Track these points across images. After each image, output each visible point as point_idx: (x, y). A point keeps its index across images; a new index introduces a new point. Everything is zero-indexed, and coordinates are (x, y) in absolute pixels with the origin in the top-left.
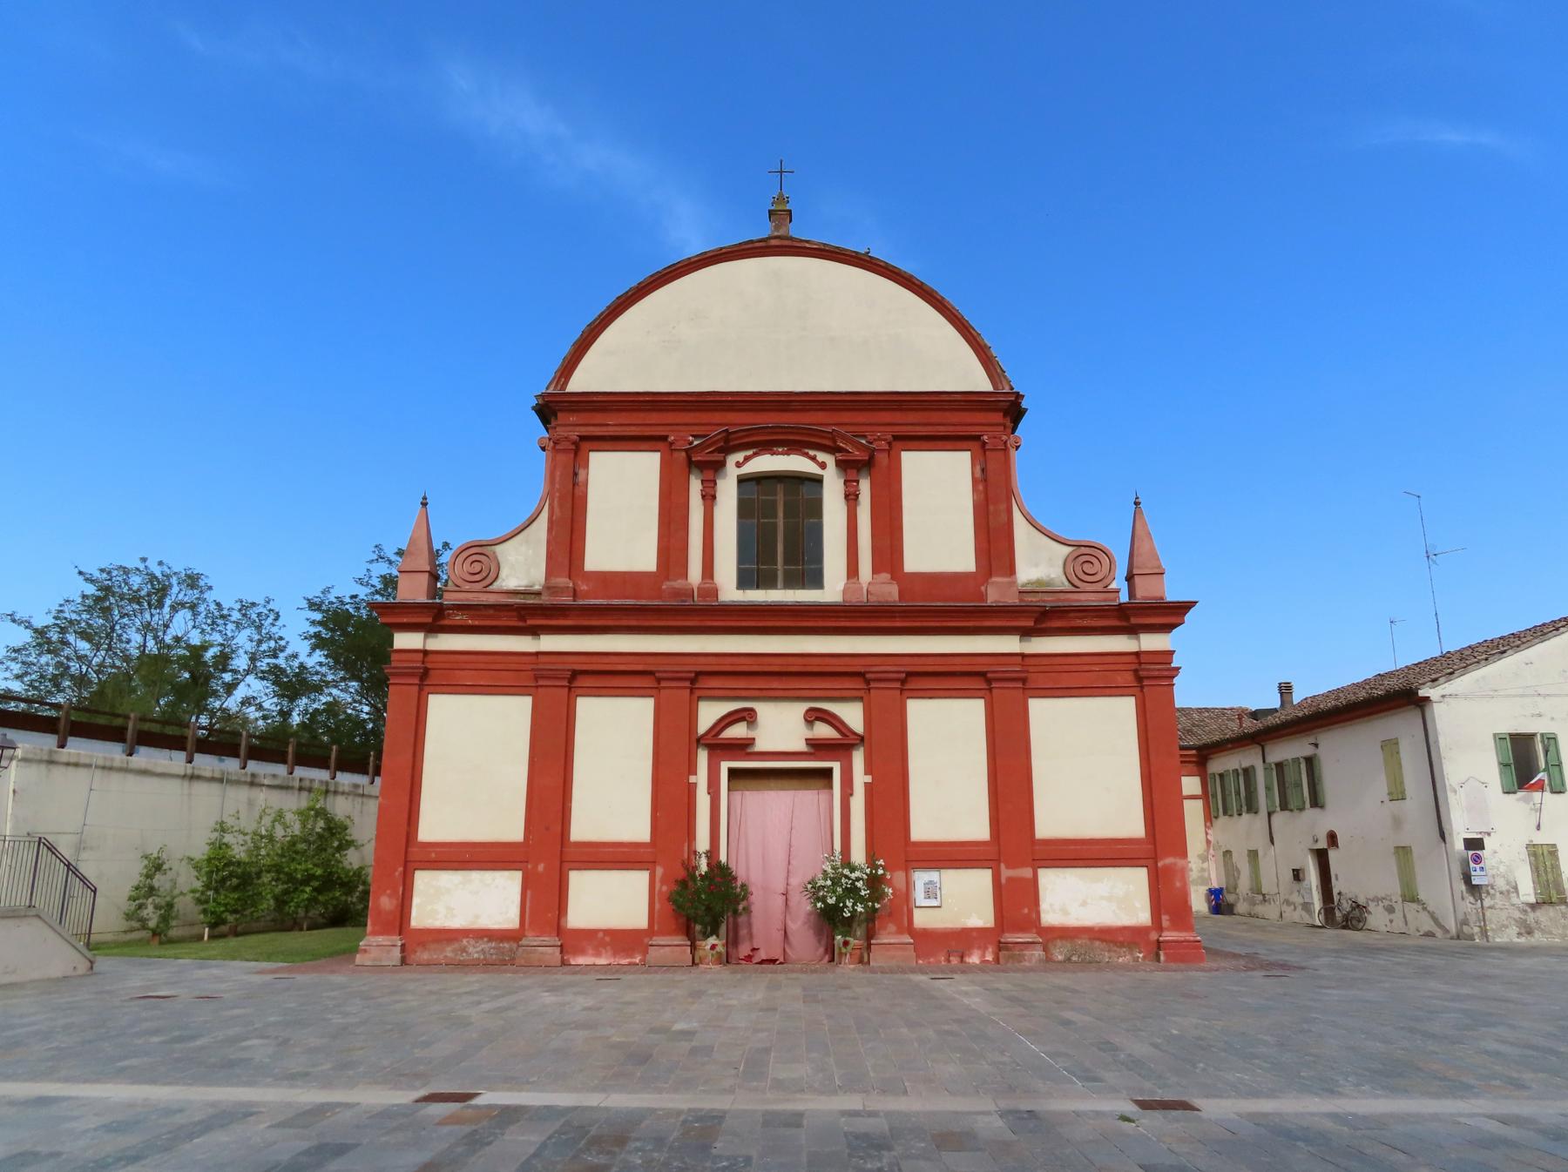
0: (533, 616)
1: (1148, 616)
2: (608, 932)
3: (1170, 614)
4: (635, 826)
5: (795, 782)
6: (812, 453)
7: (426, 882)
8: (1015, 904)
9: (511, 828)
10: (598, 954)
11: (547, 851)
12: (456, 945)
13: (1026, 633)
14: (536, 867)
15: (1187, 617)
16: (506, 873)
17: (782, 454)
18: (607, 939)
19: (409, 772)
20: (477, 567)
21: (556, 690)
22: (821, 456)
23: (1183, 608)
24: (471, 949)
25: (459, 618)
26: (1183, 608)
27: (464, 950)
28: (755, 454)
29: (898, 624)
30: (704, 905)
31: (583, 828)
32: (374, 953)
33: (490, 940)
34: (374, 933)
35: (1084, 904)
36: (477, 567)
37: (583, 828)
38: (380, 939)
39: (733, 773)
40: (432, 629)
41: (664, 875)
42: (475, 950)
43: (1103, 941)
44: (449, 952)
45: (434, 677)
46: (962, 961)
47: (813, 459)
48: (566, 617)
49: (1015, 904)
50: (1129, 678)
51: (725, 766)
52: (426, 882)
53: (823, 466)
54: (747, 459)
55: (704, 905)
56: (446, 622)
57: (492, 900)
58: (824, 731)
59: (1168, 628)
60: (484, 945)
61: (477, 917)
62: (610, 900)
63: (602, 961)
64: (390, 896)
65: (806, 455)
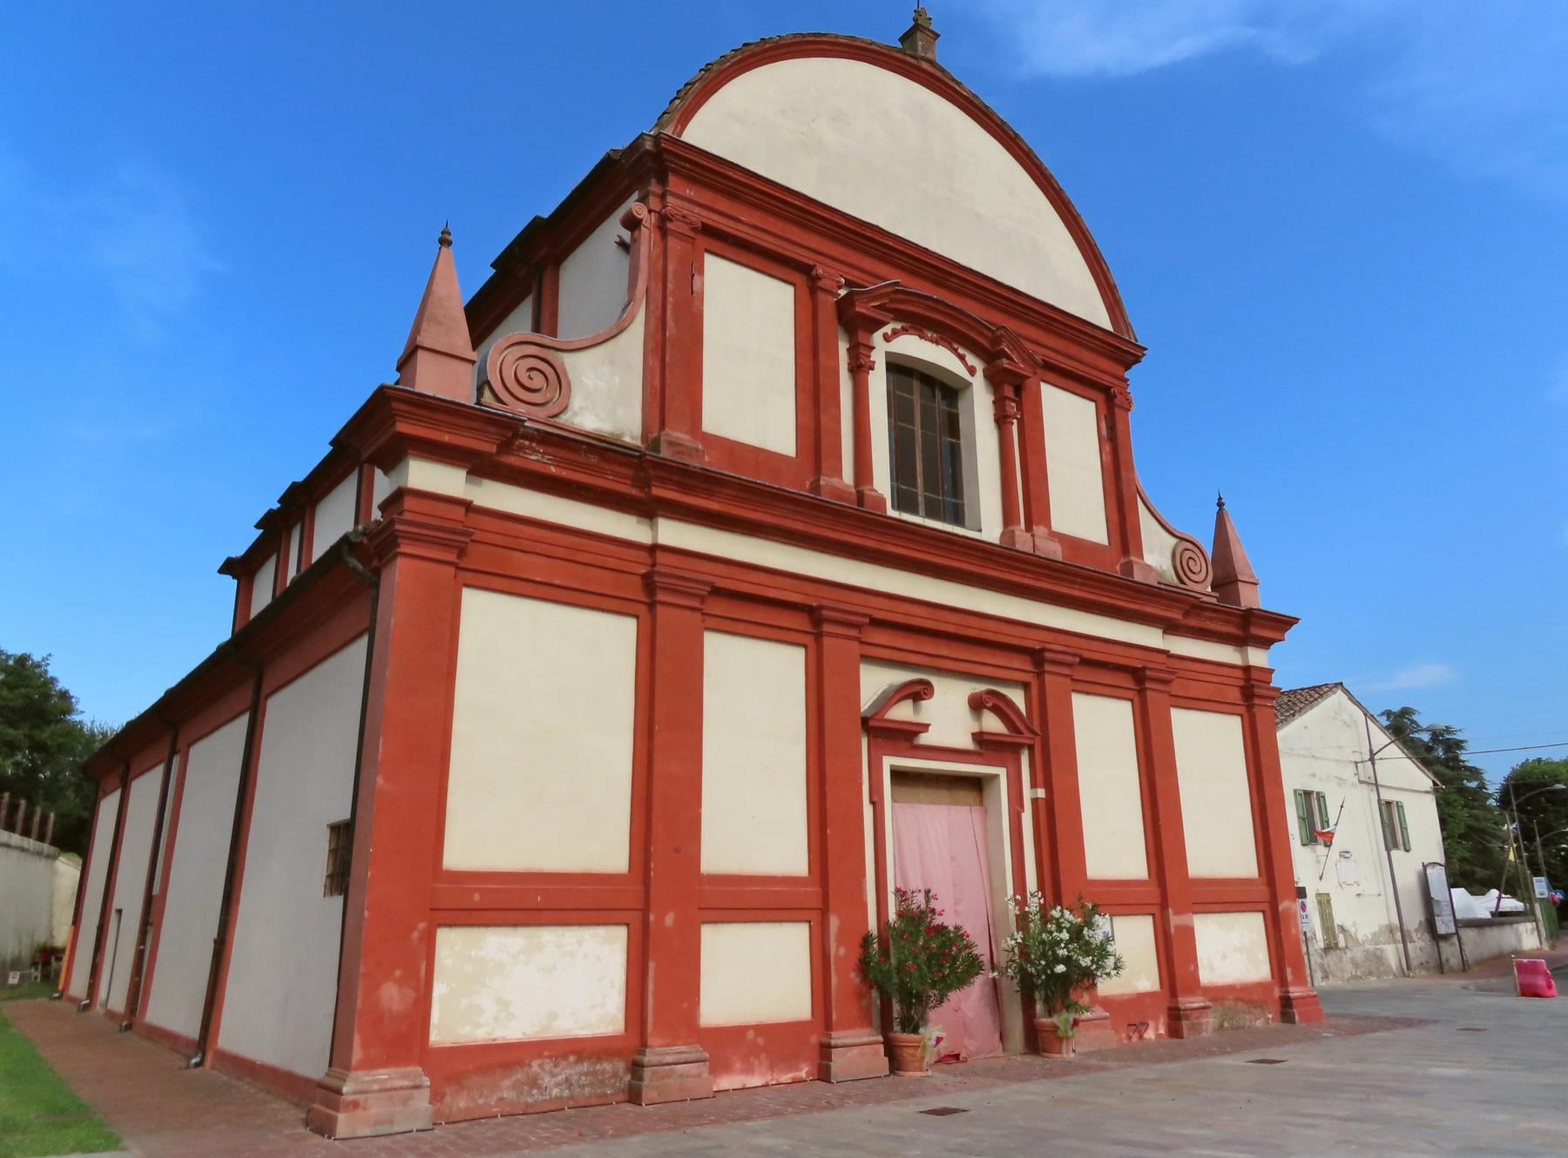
0: (664, 482)
1: (1264, 627)
2: (763, 1030)
3: (1266, 627)
4: (786, 854)
5: (944, 794)
6: (961, 351)
7: (455, 949)
8: (1174, 952)
9: (605, 848)
10: (749, 1071)
11: (659, 895)
12: (519, 1075)
13: (1171, 628)
14: (661, 918)
15: (1288, 635)
16: (601, 931)
17: (932, 341)
18: (761, 1041)
19: (659, 739)
20: (538, 381)
21: (671, 610)
22: (971, 360)
23: (1283, 623)
24: (547, 1081)
25: (535, 459)
26: (1283, 623)
27: (534, 1083)
28: (905, 331)
29: (1076, 593)
30: (892, 976)
31: (475, 840)
32: (376, 1107)
33: (580, 1059)
34: (368, 1064)
35: (1224, 957)
36: (538, 381)
37: (475, 840)
38: (383, 1074)
39: (899, 776)
40: (481, 467)
41: (841, 928)
42: (554, 1081)
43: (1242, 1000)
44: (506, 1089)
45: (477, 557)
46: (1141, 1037)
47: (962, 358)
48: (710, 494)
49: (1174, 952)
50: (1234, 695)
51: (889, 762)
52: (455, 949)
53: (972, 371)
54: (895, 333)
55: (892, 976)
56: (512, 460)
57: (563, 984)
58: (992, 724)
59: (1266, 643)
60: (571, 1070)
61: (553, 1016)
62: (756, 975)
63: (755, 1081)
64: (400, 982)
65: (955, 351)
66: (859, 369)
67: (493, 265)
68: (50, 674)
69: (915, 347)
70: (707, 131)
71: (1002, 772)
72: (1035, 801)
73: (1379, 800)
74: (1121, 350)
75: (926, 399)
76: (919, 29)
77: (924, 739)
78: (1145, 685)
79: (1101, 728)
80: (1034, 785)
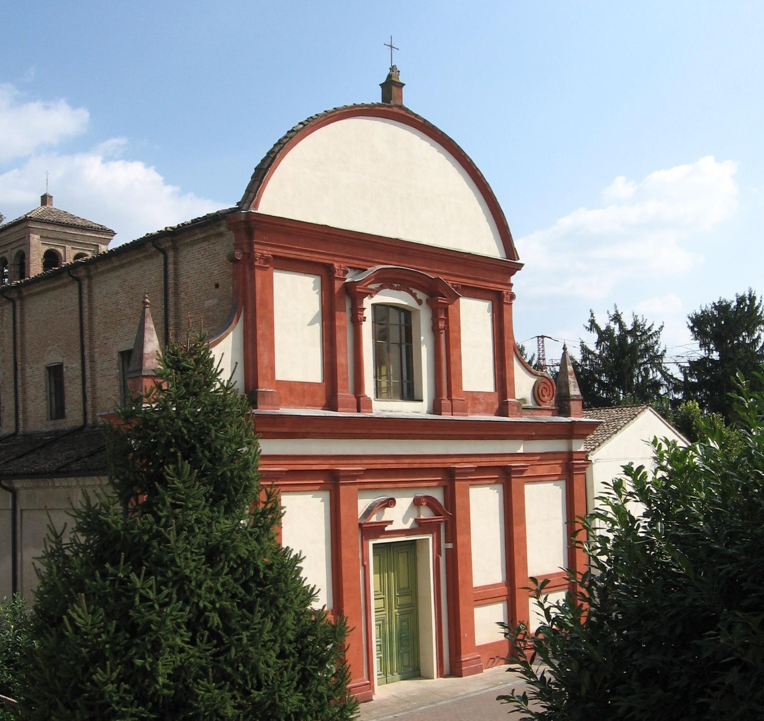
6: (414, 291)
22: (421, 295)
28: (382, 288)
53: (420, 302)
58: (426, 514)
66: (356, 322)
67: (482, 672)
68: (284, 546)
69: (386, 297)
70: (273, 202)
71: (430, 537)
72: (447, 549)
73: (35, 569)
74: (509, 265)
75: (396, 331)
76: (391, 86)
77: (388, 528)
78: (507, 477)
79: (483, 504)
80: (447, 542)
